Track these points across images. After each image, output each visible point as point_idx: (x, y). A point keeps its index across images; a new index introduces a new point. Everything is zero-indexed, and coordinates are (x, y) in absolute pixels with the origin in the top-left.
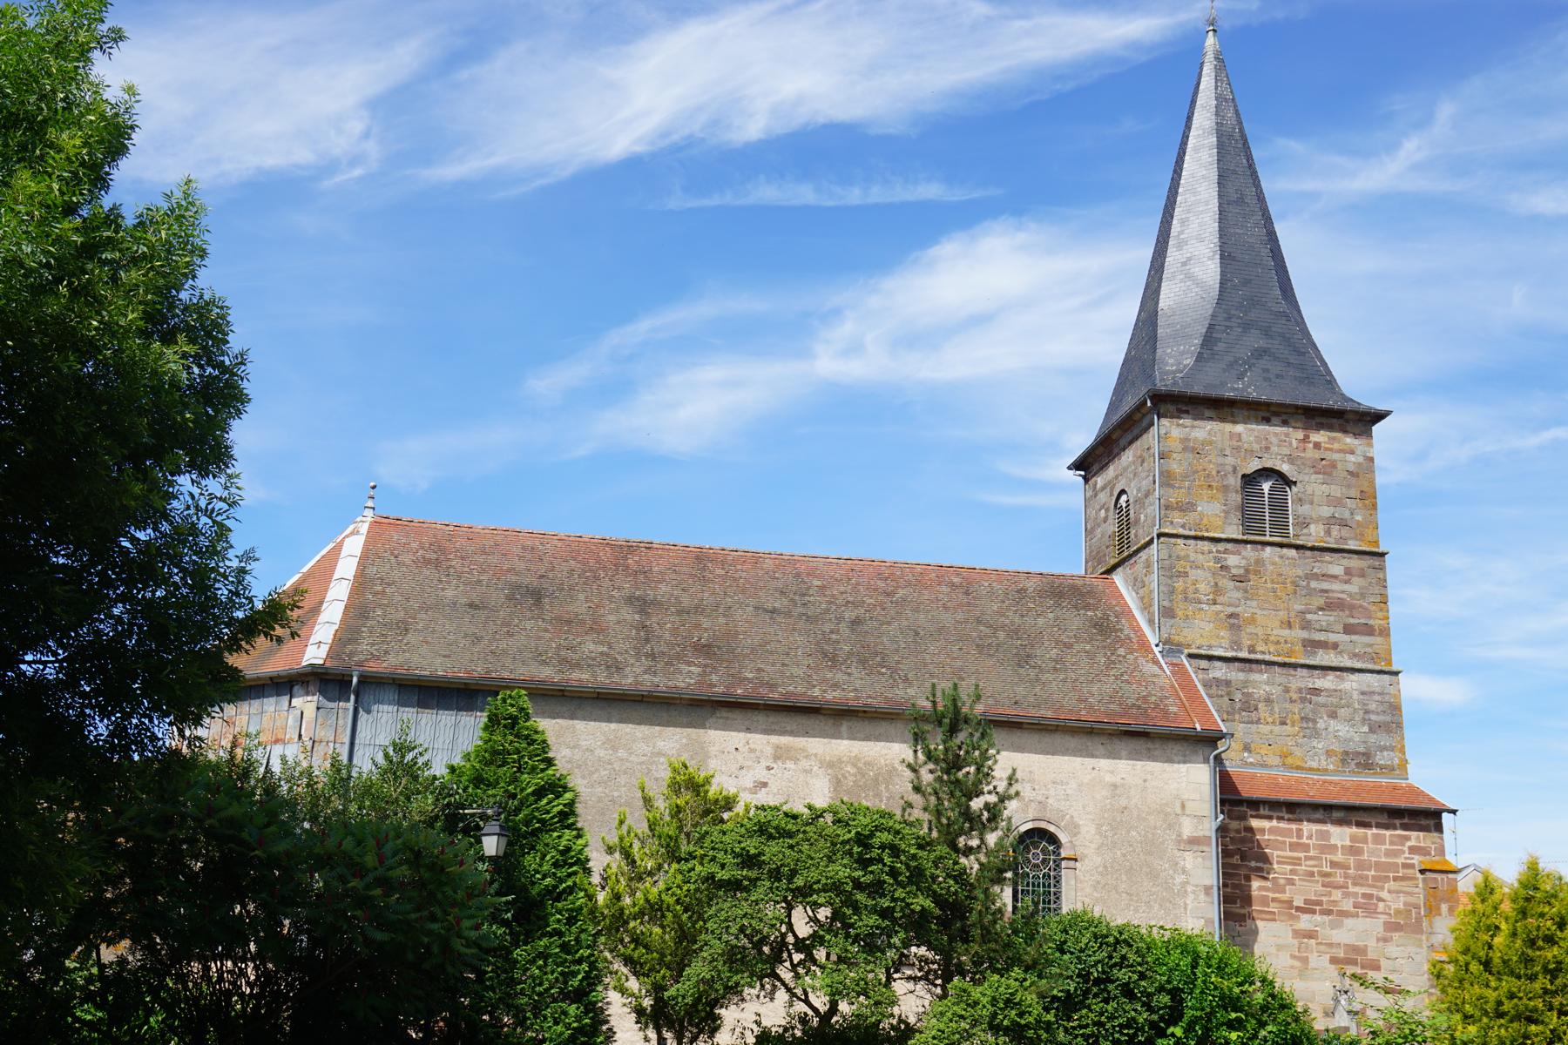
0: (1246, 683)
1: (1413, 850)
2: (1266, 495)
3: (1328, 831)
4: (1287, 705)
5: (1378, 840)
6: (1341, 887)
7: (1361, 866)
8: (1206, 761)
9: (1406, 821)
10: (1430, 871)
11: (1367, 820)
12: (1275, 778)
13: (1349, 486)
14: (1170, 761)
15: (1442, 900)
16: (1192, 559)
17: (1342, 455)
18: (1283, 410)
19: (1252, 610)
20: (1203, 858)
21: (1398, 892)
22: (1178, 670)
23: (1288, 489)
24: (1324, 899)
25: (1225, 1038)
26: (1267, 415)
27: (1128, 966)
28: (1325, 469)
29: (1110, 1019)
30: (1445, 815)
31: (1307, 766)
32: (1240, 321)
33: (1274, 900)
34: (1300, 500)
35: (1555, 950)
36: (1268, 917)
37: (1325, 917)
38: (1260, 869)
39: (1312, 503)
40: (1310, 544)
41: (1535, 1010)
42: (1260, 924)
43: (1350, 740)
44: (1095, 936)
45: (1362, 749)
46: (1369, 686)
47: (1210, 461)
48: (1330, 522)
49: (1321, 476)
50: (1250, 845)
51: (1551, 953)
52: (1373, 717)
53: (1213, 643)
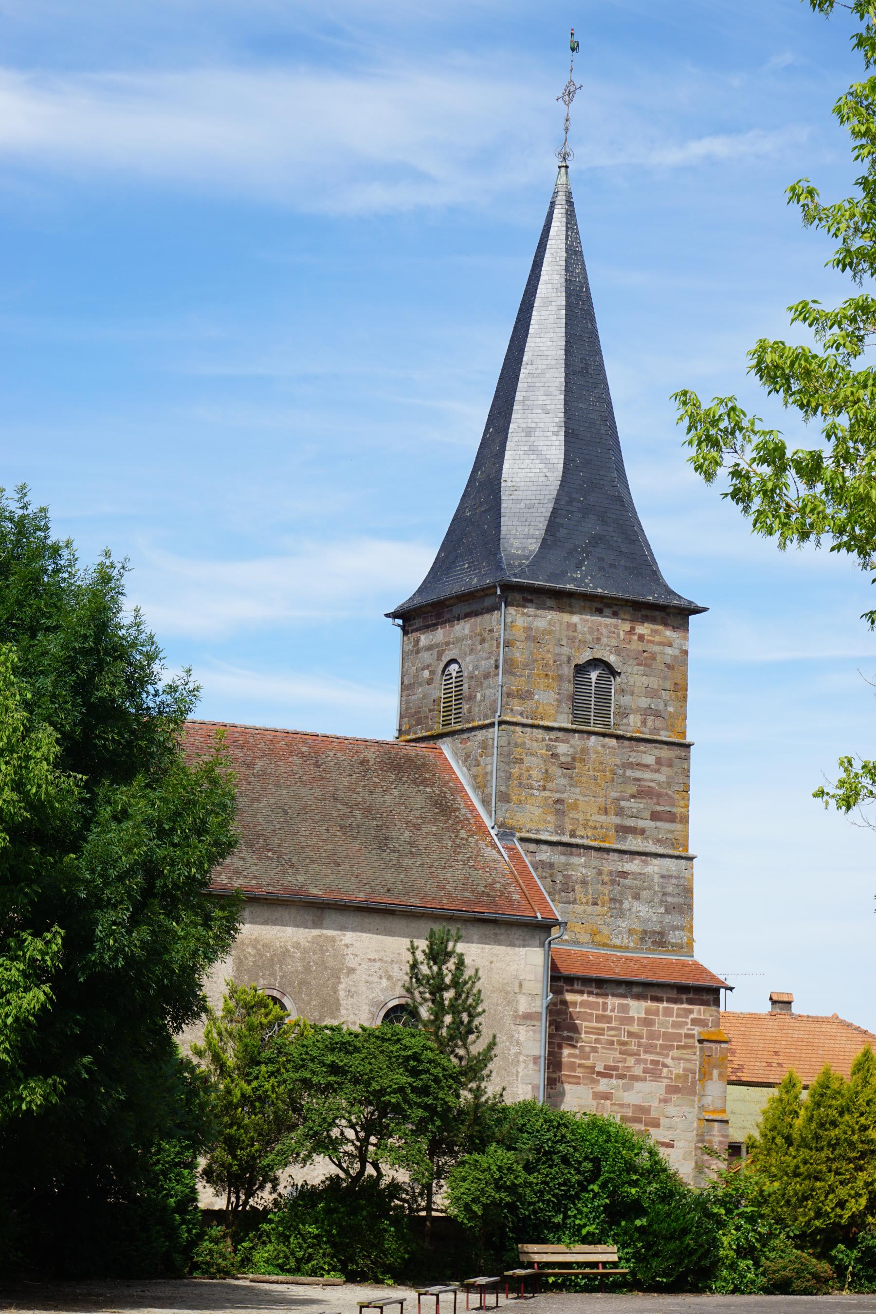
0: (566, 866)
1: (695, 1022)
2: (593, 684)
3: (628, 1005)
4: (599, 887)
5: (668, 1013)
6: (635, 1054)
7: (652, 1036)
8: (542, 945)
9: (691, 996)
10: (708, 1041)
11: (660, 995)
12: (586, 955)
13: (665, 678)
14: (512, 945)
15: (715, 1066)
16: (528, 746)
17: (662, 647)
18: (615, 602)
19: (575, 797)
20: (534, 1031)
21: (679, 1059)
22: (515, 856)
23: (612, 679)
24: (620, 1065)
25: (627, 1192)
26: (600, 606)
27: (565, 1143)
28: (646, 661)
29: (552, 1179)
30: (722, 991)
31: (612, 943)
32: (580, 505)
33: (580, 1066)
34: (623, 691)
35: (837, 1131)
36: (574, 1080)
37: (620, 1081)
38: (570, 1038)
39: (632, 694)
40: (629, 735)
41: (821, 1172)
42: (567, 1087)
43: (649, 920)
44: (546, 1121)
45: (658, 929)
46: (668, 870)
47: (549, 651)
48: (648, 712)
49: (642, 668)
50: (564, 1017)
51: (834, 1133)
52: (669, 899)
53: (541, 827)
